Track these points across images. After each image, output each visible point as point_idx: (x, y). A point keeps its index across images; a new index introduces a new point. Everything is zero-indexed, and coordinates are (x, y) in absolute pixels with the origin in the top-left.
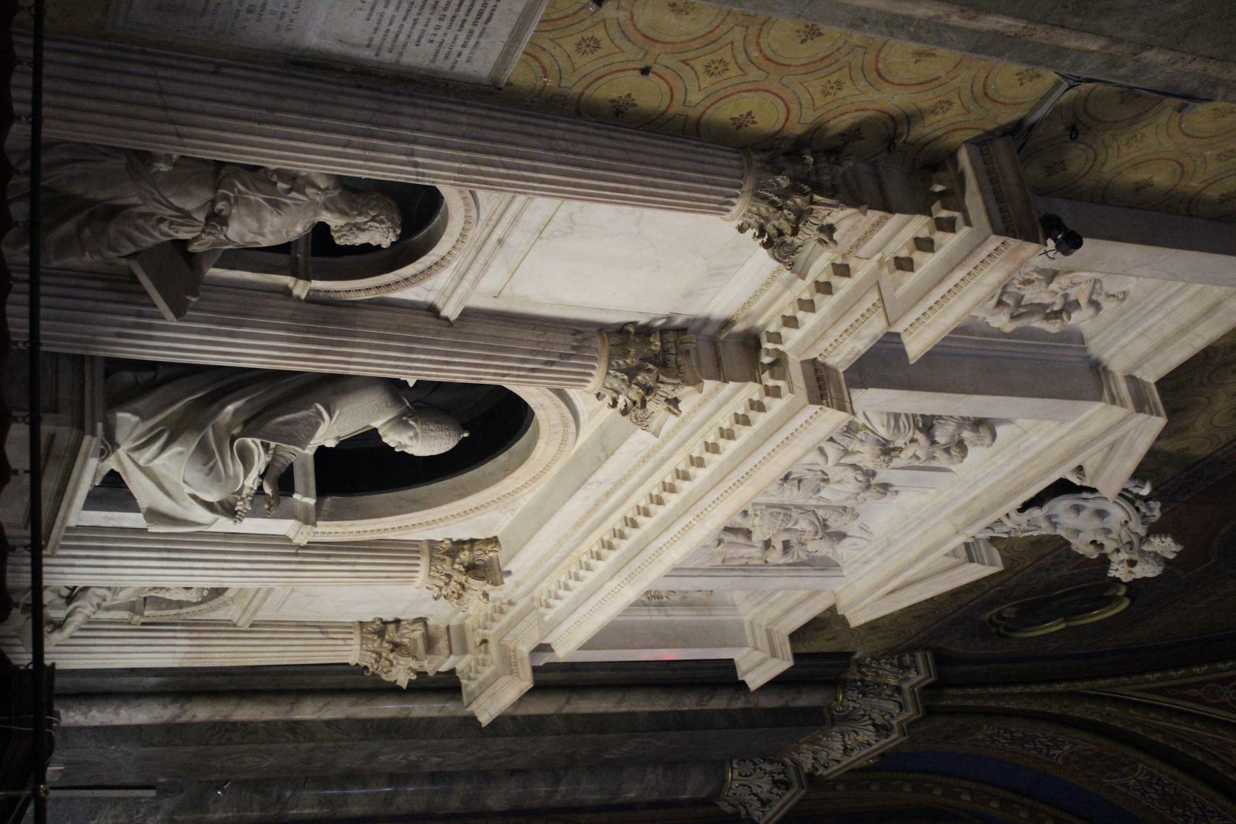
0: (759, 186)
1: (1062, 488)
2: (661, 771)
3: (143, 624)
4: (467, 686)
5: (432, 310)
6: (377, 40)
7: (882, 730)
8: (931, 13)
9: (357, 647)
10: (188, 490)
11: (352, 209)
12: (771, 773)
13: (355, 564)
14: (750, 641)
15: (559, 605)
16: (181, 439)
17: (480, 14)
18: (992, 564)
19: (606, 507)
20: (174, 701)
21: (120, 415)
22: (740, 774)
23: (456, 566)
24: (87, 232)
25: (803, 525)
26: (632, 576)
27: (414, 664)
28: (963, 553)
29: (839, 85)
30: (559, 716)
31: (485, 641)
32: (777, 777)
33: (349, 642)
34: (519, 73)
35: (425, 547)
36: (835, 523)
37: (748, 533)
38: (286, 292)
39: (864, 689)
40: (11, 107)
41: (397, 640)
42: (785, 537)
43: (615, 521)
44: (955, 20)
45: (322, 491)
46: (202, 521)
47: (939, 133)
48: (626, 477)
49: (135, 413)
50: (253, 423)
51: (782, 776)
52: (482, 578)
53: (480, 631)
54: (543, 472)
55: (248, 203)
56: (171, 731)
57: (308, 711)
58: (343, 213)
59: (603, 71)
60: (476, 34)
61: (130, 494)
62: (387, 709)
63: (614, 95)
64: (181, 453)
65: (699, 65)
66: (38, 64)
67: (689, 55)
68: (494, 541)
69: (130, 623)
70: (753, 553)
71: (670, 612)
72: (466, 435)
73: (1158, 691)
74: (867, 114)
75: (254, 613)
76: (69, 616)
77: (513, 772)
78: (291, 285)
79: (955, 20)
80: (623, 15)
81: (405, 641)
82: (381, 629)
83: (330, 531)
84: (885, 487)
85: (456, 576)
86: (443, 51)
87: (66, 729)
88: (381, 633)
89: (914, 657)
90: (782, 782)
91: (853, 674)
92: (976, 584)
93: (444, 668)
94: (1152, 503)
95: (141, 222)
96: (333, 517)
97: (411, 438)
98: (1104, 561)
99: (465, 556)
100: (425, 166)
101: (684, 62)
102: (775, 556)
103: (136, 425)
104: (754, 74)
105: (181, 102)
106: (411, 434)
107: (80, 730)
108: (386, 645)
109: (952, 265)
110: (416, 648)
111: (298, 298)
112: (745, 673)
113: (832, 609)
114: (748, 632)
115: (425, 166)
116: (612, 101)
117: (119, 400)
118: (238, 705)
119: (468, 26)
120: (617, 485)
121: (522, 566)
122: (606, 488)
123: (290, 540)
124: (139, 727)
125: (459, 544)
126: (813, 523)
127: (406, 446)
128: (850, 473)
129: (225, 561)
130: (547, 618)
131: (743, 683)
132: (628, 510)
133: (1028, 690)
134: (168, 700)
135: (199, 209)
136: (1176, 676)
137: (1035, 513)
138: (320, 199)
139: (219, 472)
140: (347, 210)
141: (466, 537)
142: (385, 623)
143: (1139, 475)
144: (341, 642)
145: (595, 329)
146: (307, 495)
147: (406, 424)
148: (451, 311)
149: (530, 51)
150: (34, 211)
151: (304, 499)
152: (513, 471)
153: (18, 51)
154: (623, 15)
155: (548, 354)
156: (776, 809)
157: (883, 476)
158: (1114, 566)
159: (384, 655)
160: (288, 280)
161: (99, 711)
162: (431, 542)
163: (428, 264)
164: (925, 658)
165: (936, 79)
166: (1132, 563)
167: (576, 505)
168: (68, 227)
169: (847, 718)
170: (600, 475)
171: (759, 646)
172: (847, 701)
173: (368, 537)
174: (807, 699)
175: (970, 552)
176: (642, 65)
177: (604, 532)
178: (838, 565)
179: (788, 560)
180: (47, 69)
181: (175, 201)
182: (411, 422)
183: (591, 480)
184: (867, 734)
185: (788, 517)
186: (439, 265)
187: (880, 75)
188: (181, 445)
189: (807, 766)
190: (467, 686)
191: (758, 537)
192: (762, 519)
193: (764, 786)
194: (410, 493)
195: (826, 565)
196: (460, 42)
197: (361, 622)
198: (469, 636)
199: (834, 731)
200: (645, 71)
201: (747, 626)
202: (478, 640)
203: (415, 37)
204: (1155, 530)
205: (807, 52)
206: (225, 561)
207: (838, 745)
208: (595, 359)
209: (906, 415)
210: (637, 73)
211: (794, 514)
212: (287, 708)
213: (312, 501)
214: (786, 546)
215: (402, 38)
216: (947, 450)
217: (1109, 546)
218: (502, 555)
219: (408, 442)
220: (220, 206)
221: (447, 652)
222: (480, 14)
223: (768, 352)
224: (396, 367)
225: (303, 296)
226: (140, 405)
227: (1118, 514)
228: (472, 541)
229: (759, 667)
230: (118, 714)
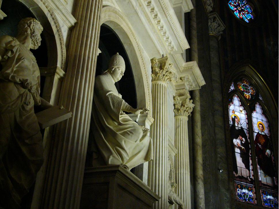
3: (176, 183)
4: (194, 88)
5: (71, 29)
9: (183, 117)
10: (138, 142)
11: (24, 34)
12: (211, 23)
13: (160, 104)
14: (180, 5)
16: (119, 141)
20: (197, 181)
21: (110, 163)
22: (211, 31)
23: (161, 72)
24: (27, 141)
27: (188, 100)
31: (181, 79)
32: (212, 21)
33: (181, 120)
35: (154, 82)
38: (61, 80)
41: (180, 105)
46: (147, 144)
49: (109, 157)
50: (115, 117)
52: (165, 63)
53: (177, 80)
57: (199, 140)
61: (139, 166)
64: (125, 141)
68: (152, 60)
69: (176, 188)
72: (118, 53)
75: (172, 145)
76: (177, 203)
78: (59, 77)
81: (181, 102)
82: (177, 110)
83: (149, 105)
85: (164, 73)
88: (178, 110)
90: (214, 19)
95: (24, 118)
97: (119, 70)
99: (157, 70)
103: (114, 156)
106: (117, 69)
108: (182, 108)
110: (183, 99)
111: (64, 75)
112: (189, 8)
114: (177, 6)
117: (104, 161)
118: (198, 161)
123: (152, 125)
124: (205, 192)
125: (153, 72)
127: (122, 72)
129: (159, 145)
130: (176, 50)
131: (191, 10)
134: (197, 183)
139: (132, 130)
140: (23, 37)
141: (151, 70)
142: (175, 109)
144: (181, 122)
147: (114, 71)
148: (73, 21)
152: (130, 41)
156: (221, 23)
159: (185, 109)
160: (56, 78)
161: (201, 204)
168: (24, 150)
173: (151, 99)
182: (113, 69)
183: (135, 8)
188: (122, 141)
190: (194, 88)
193: (215, 24)
197: (175, 116)
198: (179, 84)
201: (175, 6)
202: (180, 81)
206: (159, 145)
212: (199, 147)
221: (184, 90)
224: (94, 43)
225: (64, 72)
226: (106, 155)
230: (201, 198)
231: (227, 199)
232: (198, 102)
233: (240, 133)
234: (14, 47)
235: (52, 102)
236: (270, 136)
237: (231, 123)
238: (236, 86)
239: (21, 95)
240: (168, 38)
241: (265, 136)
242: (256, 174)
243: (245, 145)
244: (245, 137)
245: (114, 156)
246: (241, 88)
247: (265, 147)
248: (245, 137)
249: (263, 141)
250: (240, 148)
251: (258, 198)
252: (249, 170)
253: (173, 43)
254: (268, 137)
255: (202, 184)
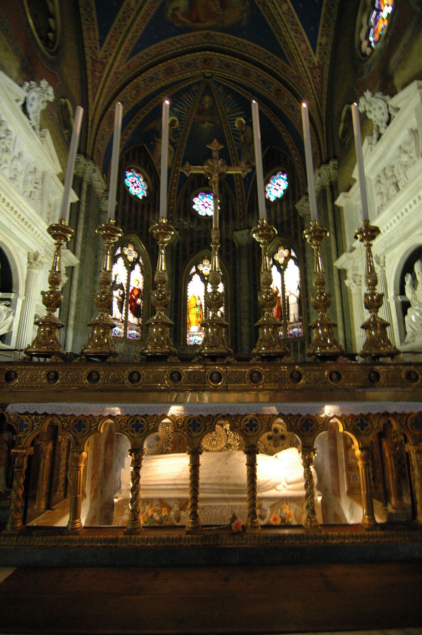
1: (24, 107)
7: (94, 171)
15: (47, 241)
18: (46, 132)
19: (18, 225)
25: (30, 178)
26: (38, 222)
28: (42, 139)
30: (82, 246)
36: (32, 169)
37: (32, 192)
39: (84, 173)
42: (33, 183)
43: (22, 224)
45: (11, 291)
48: (8, 219)
54: (7, 239)
56: (75, 328)
62: (75, 283)
68: (28, 253)
70: (37, 192)
77: (96, 257)
83: (22, 290)
84: (20, 154)
87: (72, 350)
91: (80, 175)
92: (53, 138)
93: (64, 269)
96: (18, 289)
98: (48, 102)
99: (32, 261)
102: (39, 186)
107: (73, 347)
113: (57, 175)
120: (10, 221)
121: (34, 248)
122: (11, 225)
124: (74, 335)
125: (29, 262)
128: (14, 162)
132: (19, 220)
136: (90, 93)
137: (31, 116)
141: (27, 260)
143: (21, 86)
146: (11, 295)
149: (233, 122)
151: (12, 296)
157: (16, 154)
158: (49, 99)
166: (48, 94)
167: (17, 233)
169: (91, 179)
170: (7, 225)
172: (86, 178)
174: (85, 187)
175: (42, 136)
177: (26, 227)
179: (41, 183)
184: (95, 175)
185: (27, 181)
189: (103, 191)
191: (32, 190)
194: (13, 271)
195: (44, 174)
199: (94, 182)
204: (39, 85)
207: (98, 183)
211: (27, 179)
213: (13, 294)
214: (36, 183)
216: (8, 135)
217: (43, 99)
218: (32, 252)
227: (33, 94)
228: (28, 258)
229: (73, 198)
233: (121, 286)
236: (143, 290)
237: (113, 279)
238: (122, 250)
240: (42, 238)
241: (139, 290)
242: (126, 317)
243: (123, 296)
244: (123, 289)
246: (126, 252)
247: (137, 297)
248: (123, 289)
249: (136, 293)
250: (117, 298)
251: (125, 333)
252: (122, 313)
253: (47, 241)
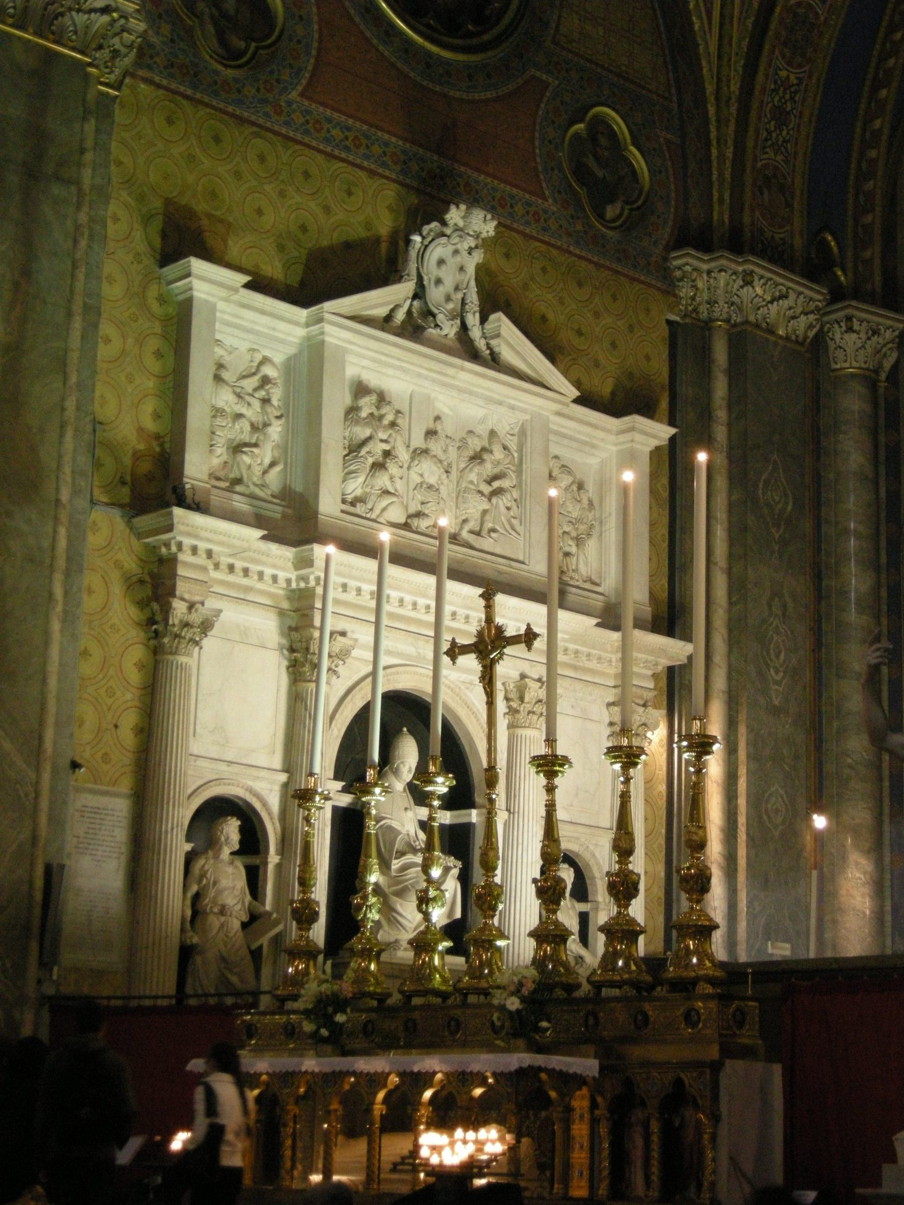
0: (171, 653)
2: (841, 436)
6: (115, 855)
8: (505, 421)
14: (629, 445)
17: (95, 813)
18: (499, 320)
22: (846, 361)
24: (235, 970)
29: (112, 626)
34: (125, 785)
35: (511, 731)
38: (279, 866)
40: (812, 960)
44: (59, 608)
47: (135, 558)
51: (843, 324)
55: (215, 897)
58: (221, 848)
59: (119, 746)
60: (106, 812)
63: (132, 736)
64: (401, 905)
65: (109, 701)
66: (140, 998)
67: (105, 708)
71: (607, 514)
72: (405, 729)
73: (709, 14)
74: (128, 604)
79: (59, 608)
80: (88, 748)
86: (118, 824)
89: (676, 267)
94: (424, 233)
100: (173, 824)
101: (109, 709)
103: (385, 931)
104: (112, 671)
105: (150, 939)
106: (401, 766)
109: (196, 537)
111: (281, 859)
114: (624, 447)
115: (173, 824)
116: (136, 736)
119: (102, 816)
126: (471, 469)
133: (714, 142)
135: (218, 919)
138: (211, 862)
145: (294, 688)
146: (470, 815)
150: (231, 994)
153: (136, 1005)
154: (88, 748)
155: (305, 718)
162: (508, 728)
163: (251, 796)
164: (675, 258)
165: (103, 577)
171: (630, 438)
176: (113, 729)
178: (523, 424)
180: (142, 993)
181: (215, 931)
186: (251, 791)
187: (104, 607)
192: (468, 509)
194: (467, 749)
196: (112, 818)
200: (116, 726)
203: (111, 839)
205: (97, 654)
208: (307, 690)
209: (345, 468)
210: (118, 730)
215: (113, 844)
219: (407, 767)
220: (216, 910)
222: (95, 813)
223: (298, 585)
231: (862, 876)
232: (720, 667)
234: (207, 871)
235: (268, 907)
239: (222, 925)
245: (385, 931)
254: (134, 1144)
255: (720, 874)
